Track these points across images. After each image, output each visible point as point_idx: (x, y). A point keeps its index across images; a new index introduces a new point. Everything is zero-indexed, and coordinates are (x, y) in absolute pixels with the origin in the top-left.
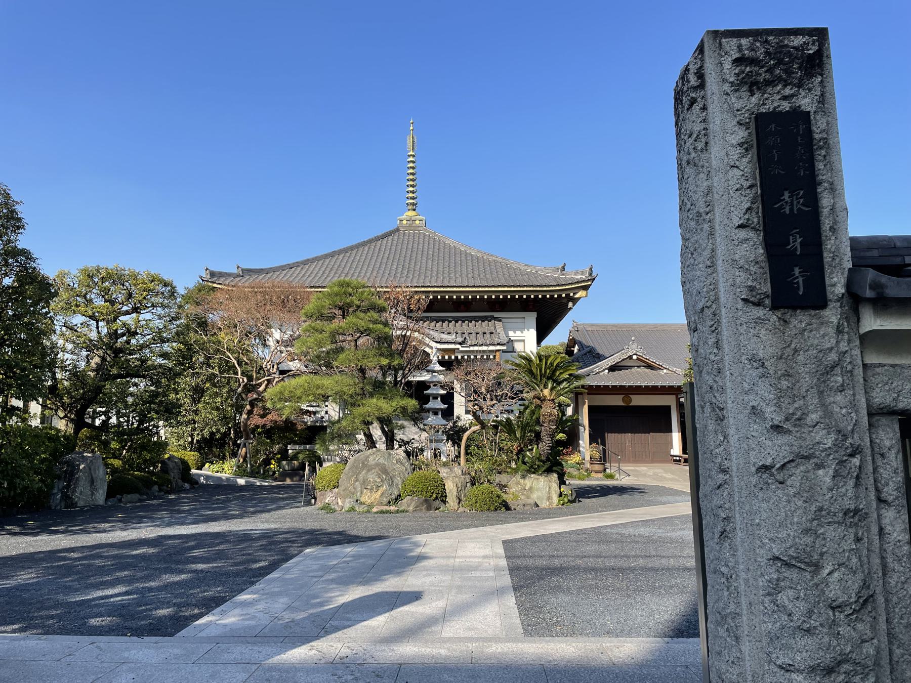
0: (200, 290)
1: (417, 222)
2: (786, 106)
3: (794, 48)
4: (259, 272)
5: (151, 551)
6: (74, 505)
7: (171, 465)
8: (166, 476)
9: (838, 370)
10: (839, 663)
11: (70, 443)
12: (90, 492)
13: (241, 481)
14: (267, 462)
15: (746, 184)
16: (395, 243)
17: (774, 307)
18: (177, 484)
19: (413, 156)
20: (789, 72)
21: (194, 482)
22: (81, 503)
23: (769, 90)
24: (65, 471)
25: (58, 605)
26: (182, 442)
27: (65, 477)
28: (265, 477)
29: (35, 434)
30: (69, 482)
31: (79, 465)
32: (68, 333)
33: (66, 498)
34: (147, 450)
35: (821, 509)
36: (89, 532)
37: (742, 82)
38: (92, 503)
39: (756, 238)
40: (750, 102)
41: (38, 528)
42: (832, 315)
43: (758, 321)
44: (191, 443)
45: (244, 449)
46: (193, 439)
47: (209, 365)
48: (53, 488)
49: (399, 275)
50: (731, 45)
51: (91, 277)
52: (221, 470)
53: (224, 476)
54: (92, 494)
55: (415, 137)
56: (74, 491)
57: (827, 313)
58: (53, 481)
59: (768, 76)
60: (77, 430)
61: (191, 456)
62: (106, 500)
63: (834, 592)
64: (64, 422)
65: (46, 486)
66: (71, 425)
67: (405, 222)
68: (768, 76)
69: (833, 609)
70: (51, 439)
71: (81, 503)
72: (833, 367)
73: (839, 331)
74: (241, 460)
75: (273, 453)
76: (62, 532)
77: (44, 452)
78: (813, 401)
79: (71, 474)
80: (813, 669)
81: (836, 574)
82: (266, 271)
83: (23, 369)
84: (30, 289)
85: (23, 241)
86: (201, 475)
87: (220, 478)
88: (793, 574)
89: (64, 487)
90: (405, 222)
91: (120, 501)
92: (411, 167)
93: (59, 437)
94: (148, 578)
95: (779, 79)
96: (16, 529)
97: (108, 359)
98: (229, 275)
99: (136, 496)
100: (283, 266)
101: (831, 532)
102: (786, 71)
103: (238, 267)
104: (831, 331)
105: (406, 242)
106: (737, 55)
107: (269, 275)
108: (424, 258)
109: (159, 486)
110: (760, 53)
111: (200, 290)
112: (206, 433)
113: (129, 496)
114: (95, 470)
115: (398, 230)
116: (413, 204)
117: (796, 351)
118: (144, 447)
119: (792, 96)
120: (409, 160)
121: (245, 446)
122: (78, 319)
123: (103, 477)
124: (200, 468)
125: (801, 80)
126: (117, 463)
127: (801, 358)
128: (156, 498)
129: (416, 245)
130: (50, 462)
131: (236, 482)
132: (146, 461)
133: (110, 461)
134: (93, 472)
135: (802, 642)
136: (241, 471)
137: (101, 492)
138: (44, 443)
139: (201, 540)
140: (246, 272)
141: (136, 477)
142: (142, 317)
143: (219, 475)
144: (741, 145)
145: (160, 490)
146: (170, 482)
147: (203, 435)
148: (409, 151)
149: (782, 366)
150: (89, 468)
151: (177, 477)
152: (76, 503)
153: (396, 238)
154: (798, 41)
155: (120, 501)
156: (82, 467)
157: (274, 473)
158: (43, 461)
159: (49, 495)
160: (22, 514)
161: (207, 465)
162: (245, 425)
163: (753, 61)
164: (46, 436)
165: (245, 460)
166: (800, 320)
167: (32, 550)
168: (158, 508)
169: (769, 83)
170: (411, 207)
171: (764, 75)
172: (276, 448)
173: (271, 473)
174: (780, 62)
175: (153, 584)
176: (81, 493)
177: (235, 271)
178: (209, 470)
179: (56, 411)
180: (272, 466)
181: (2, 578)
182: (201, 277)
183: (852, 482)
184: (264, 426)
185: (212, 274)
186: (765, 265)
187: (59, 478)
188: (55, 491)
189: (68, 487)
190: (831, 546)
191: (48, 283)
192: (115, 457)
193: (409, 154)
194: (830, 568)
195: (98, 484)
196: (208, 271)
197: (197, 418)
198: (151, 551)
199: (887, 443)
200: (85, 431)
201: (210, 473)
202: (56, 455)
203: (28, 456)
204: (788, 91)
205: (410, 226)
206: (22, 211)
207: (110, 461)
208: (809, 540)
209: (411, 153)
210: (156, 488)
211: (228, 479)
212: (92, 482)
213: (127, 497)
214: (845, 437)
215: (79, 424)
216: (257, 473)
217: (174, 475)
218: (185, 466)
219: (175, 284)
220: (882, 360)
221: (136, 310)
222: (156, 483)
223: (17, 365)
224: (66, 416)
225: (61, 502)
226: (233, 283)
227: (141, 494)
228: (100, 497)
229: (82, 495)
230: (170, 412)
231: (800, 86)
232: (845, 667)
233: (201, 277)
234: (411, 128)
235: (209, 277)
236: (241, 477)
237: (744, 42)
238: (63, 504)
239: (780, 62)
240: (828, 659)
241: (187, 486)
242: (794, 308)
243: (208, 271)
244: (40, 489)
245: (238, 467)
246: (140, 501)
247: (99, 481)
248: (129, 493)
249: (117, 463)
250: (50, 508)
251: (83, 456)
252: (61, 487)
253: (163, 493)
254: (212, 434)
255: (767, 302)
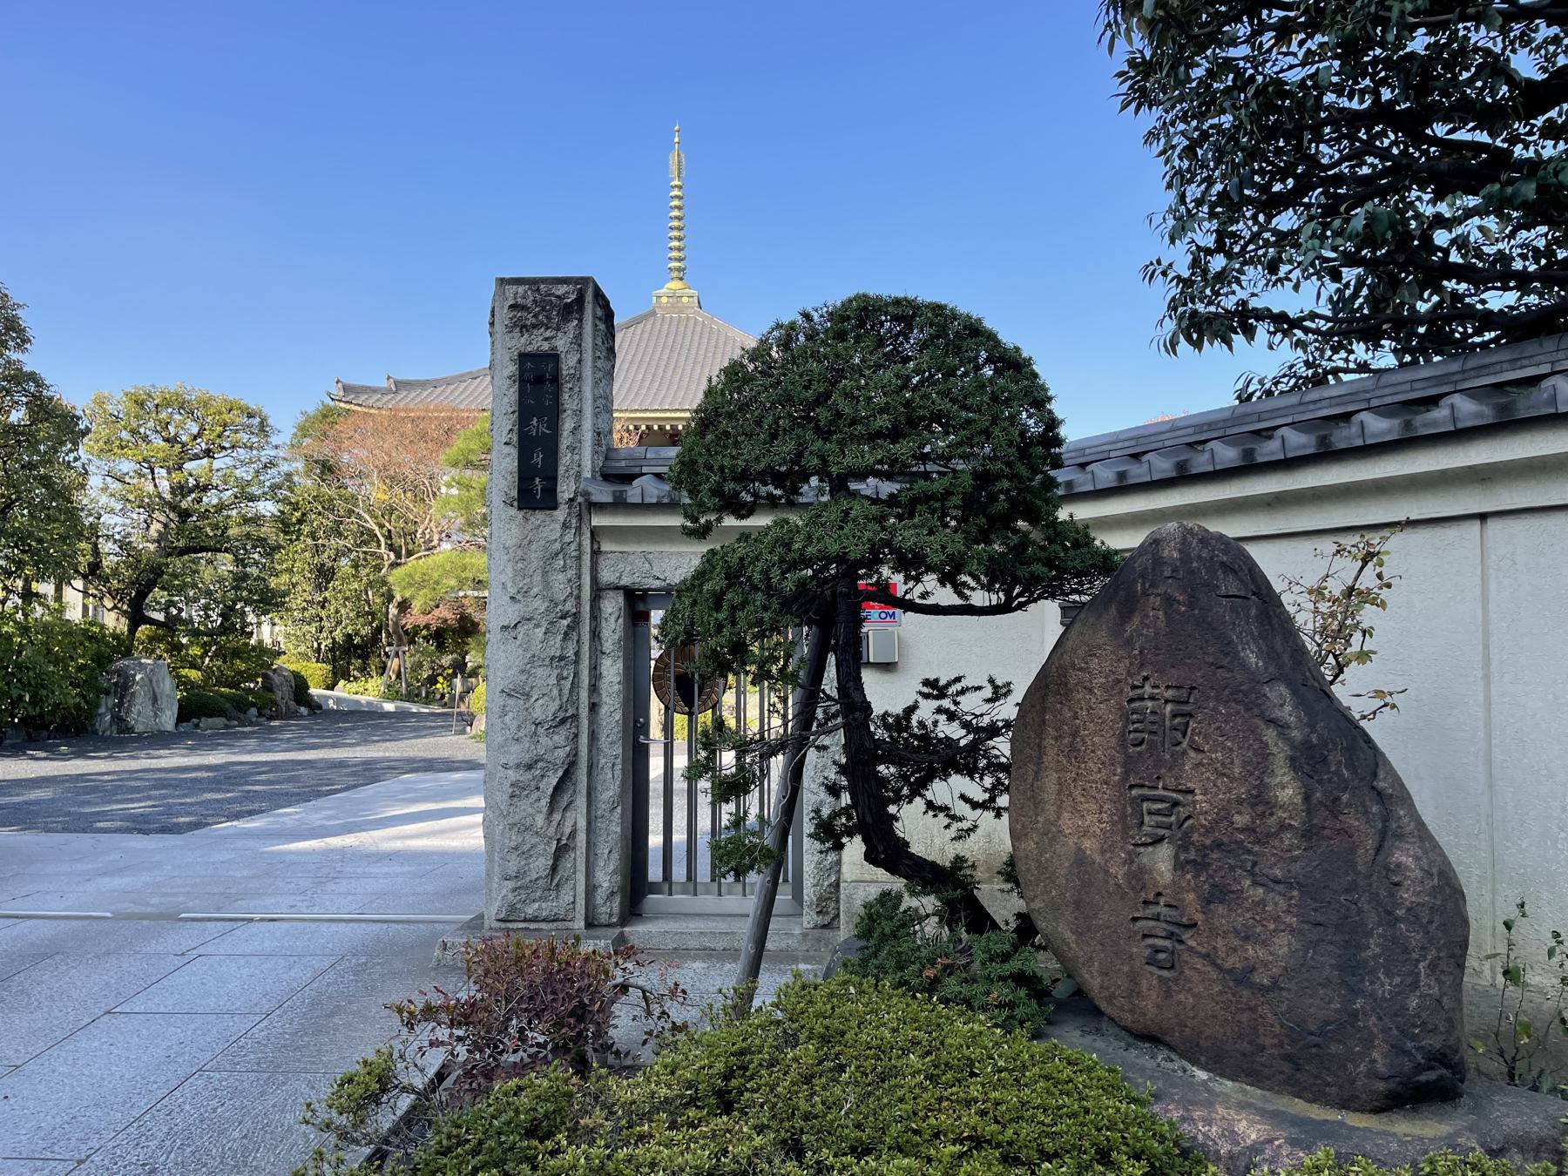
0: (325, 416)
1: (685, 300)
2: (546, 346)
3: (557, 297)
4: (423, 385)
5: (205, 775)
6: (130, 730)
7: (276, 679)
8: (269, 695)
9: (561, 556)
10: (536, 762)
11: (124, 647)
12: (152, 714)
13: (389, 707)
14: (432, 680)
15: (511, 410)
16: (646, 335)
17: (520, 508)
18: (288, 707)
19: (680, 187)
20: (549, 318)
21: (315, 707)
22: (140, 728)
23: (535, 332)
24: (116, 684)
25: (68, 814)
26: (302, 648)
27: (116, 692)
28: (428, 700)
29: (69, 630)
30: (121, 698)
31: (135, 675)
32: (115, 486)
33: (118, 720)
34: (240, 658)
35: (534, 656)
36: (138, 758)
37: (515, 325)
38: (156, 728)
39: (514, 452)
40: (521, 342)
41: (72, 753)
42: (561, 514)
43: (512, 518)
44: (318, 650)
45: (396, 660)
46: (319, 645)
47: (340, 535)
48: (98, 706)
49: (644, 391)
50: (511, 290)
51: (141, 404)
52: (361, 690)
53: (363, 699)
54: (156, 715)
55: (683, 155)
56: (128, 711)
57: (556, 513)
58: (98, 696)
59: (534, 321)
60: (133, 629)
61: (315, 672)
62: (177, 725)
63: (538, 714)
64: (113, 615)
65: (87, 703)
66: (123, 620)
67: (664, 300)
68: (534, 321)
69: (537, 725)
70: (91, 638)
71: (140, 728)
72: (557, 554)
73: (565, 526)
74: (394, 677)
75: (441, 666)
76: (105, 758)
77: (83, 656)
78: (537, 578)
79: (123, 688)
80: (518, 766)
81: (540, 701)
82: (435, 384)
83: (40, 541)
84: (44, 430)
85: (29, 361)
86: (330, 697)
87: (357, 702)
88: (511, 702)
89: (115, 705)
90: (664, 300)
91: (197, 726)
92: (676, 207)
93: (104, 636)
94: (185, 796)
95: (542, 324)
96: (43, 755)
97: (172, 525)
98: (374, 391)
99: (220, 721)
100: (462, 376)
101: (540, 672)
102: (547, 317)
103: (389, 378)
104: (558, 526)
105: (664, 334)
106: (512, 302)
107: (439, 390)
108: (690, 362)
109: (259, 709)
110: (529, 302)
111: (325, 416)
112: (338, 635)
113: (210, 720)
114: (158, 681)
115: (653, 313)
116: (679, 270)
117: (530, 542)
118: (236, 653)
119: (552, 338)
120: (672, 194)
121: (397, 655)
122: (127, 466)
123: (172, 696)
124: (331, 687)
125: (558, 325)
126: (194, 675)
127: (533, 547)
128: (251, 724)
129: (679, 339)
130: (93, 670)
131: (382, 707)
132: (240, 673)
133: (184, 672)
134: (155, 685)
135: (515, 748)
136: (392, 694)
137: (168, 713)
138: (82, 644)
139: (274, 766)
140: (401, 385)
141: (222, 695)
142: (217, 464)
143: (358, 697)
144: (510, 378)
145: (260, 715)
146: (275, 703)
147: (333, 639)
148: (673, 180)
149: (520, 552)
150: (149, 681)
151: (286, 698)
152: (133, 728)
153: (649, 327)
154: (561, 290)
155: (197, 726)
156: (138, 677)
157: (443, 696)
158: (81, 668)
159: (92, 712)
160: (55, 738)
161: (342, 683)
162: (396, 624)
163: (523, 308)
164: (90, 636)
165: (399, 676)
166: (540, 516)
167: (56, 773)
168: (246, 736)
169: (534, 326)
170: (675, 274)
171: (531, 320)
172: (446, 660)
173: (438, 696)
174: (543, 309)
175: (188, 800)
176: (139, 712)
177: (384, 384)
178: (344, 690)
179: (101, 599)
180: (439, 686)
181: (4, 795)
182: (329, 394)
183: (560, 637)
184: (427, 627)
185: (347, 389)
186: (516, 475)
187: (107, 693)
188: (102, 710)
189: (120, 705)
190: (539, 682)
191: (75, 416)
192: (193, 666)
193: (673, 183)
194: (536, 697)
195: (163, 702)
196: (340, 385)
197: (323, 614)
198: (205, 775)
199: (610, 611)
200: (143, 631)
201: (345, 695)
202: (101, 661)
203: (56, 661)
204: (548, 334)
205: (673, 306)
206: (25, 318)
207: (184, 672)
208: (524, 678)
209: (676, 182)
210: (254, 711)
211: (369, 703)
212: (155, 700)
213: (205, 722)
214: (556, 605)
215: (137, 617)
216: (417, 696)
217: (283, 695)
218: (300, 685)
219: (266, 411)
220: (614, 548)
221: (208, 453)
222: (253, 705)
223: (31, 535)
224: (115, 607)
225: (111, 725)
226: (379, 404)
227: (229, 719)
228: (168, 720)
229: (140, 715)
230: (269, 601)
231: (558, 329)
232: (540, 764)
233: (329, 394)
234: (676, 140)
235: (341, 393)
236: (393, 700)
237: (521, 289)
238: (114, 728)
239: (543, 309)
240: (527, 759)
241: (303, 710)
242: (534, 509)
243: (340, 385)
244: (78, 707)
245: (389, 686)
246: (226, 727)
247: (165, 699)
248: (210, 716)
249: (194, 675)
250: (95, 733)
251: (141, 664)
252: (110, 706)
253: (263, 719)
254: (349, 637)
255: (515, 504)
